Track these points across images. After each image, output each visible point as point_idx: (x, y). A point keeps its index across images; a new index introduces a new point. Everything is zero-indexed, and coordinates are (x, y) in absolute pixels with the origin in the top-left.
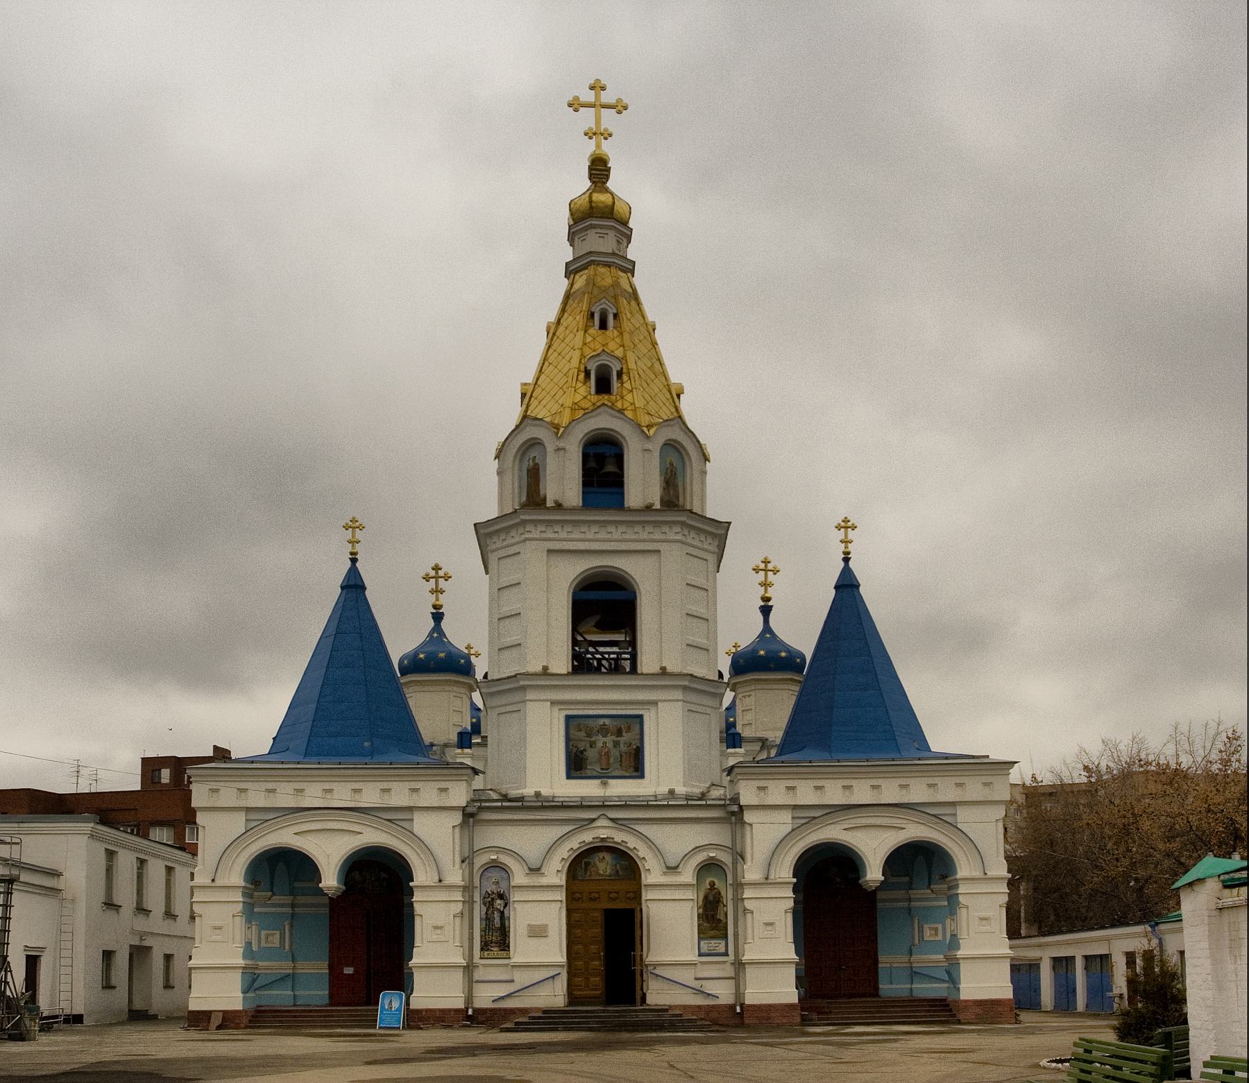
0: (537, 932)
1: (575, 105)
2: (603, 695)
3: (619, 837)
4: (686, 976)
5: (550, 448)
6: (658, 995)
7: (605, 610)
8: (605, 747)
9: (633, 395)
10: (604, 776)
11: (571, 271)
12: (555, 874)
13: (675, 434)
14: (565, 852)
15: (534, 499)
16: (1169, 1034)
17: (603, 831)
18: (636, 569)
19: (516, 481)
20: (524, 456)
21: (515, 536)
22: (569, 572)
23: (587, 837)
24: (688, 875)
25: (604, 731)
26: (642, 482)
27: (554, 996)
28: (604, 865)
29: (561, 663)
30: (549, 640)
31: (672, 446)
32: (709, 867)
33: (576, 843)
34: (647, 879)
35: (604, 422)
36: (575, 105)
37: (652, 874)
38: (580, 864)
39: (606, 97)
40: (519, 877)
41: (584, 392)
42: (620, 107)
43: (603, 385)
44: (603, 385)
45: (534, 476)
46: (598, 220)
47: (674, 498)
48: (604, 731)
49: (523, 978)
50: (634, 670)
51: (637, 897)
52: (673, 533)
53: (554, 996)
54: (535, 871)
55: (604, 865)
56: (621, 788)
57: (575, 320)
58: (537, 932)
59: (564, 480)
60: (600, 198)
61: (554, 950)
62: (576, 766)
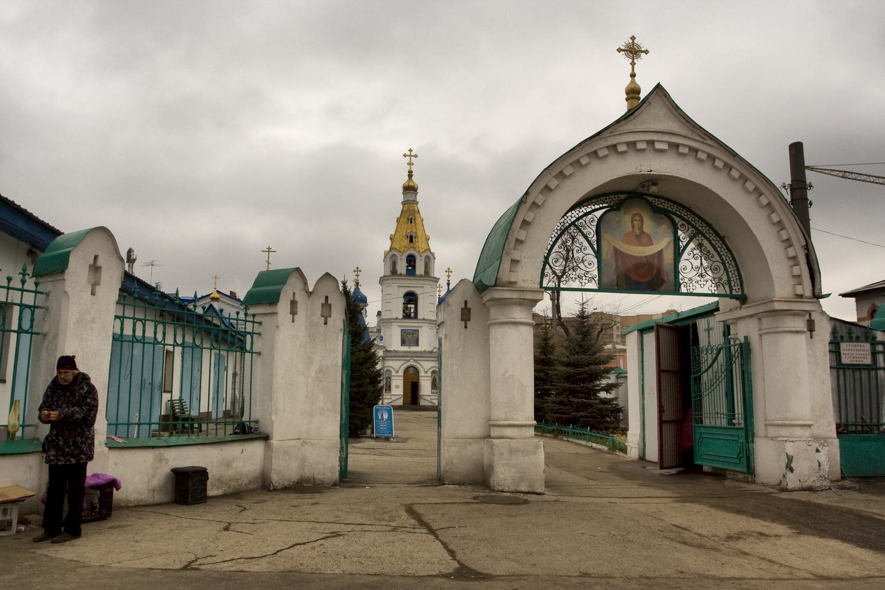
0: (397, 387)
1: (405, 155)
2: (410, 324)
3: (415, 364)
4: (428, 398)
5: (399, 258)
6: (422, 403)
7: (411, 298)
8: (410, 338)
9: (420, 243)
10: (409, 346)
11: (404, 203)
12: (401, 373)
13: (428, 253)
14: (403, 368)
15: (394, 272)
16: (201, 474)
17: (412, 363)
18: (417, 291)
19: (389, 264)
20: (391, 258)
21: (390, 282)
22: (404, 291)
23: (408, 364)
24: (429, 374)
25: (410, 334)
26: (420, 269)
27: (400, 402)
28: (411, 371)
29: (400, 316)
30: (397, 310)
31: (427, 257)
32: (434, 372)
33: (405, 365)
34: (421, 374)
35: (411, 252)
36: (405, 155)
37: (422, 374)
38: (406, 370)
39: (413, 153)
40: (394, 373)
41: (406, 242)
42: (416, 156)
43: (411, 241)
44: (411, 241)
45: (394, 264)
46: (410, 189)
47: (427, 273)
48: (410, 334)
49: (394, 398)
50: (416, 317)
51: (418, 378)
52: (427, 282)
53: (400, 402)
54: (397, 372)
55: (411, 371)
56: (414, 349)
57: (404, 220)
58: (397, 387)
59: (402, 267)
60: (411, 184)
61: (400, 391)
62: (403, 343)
